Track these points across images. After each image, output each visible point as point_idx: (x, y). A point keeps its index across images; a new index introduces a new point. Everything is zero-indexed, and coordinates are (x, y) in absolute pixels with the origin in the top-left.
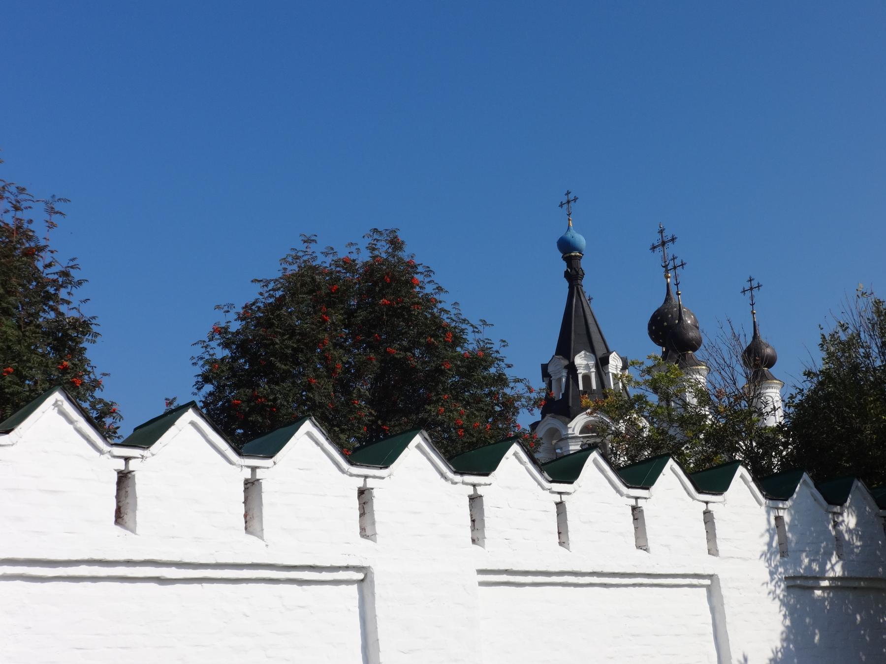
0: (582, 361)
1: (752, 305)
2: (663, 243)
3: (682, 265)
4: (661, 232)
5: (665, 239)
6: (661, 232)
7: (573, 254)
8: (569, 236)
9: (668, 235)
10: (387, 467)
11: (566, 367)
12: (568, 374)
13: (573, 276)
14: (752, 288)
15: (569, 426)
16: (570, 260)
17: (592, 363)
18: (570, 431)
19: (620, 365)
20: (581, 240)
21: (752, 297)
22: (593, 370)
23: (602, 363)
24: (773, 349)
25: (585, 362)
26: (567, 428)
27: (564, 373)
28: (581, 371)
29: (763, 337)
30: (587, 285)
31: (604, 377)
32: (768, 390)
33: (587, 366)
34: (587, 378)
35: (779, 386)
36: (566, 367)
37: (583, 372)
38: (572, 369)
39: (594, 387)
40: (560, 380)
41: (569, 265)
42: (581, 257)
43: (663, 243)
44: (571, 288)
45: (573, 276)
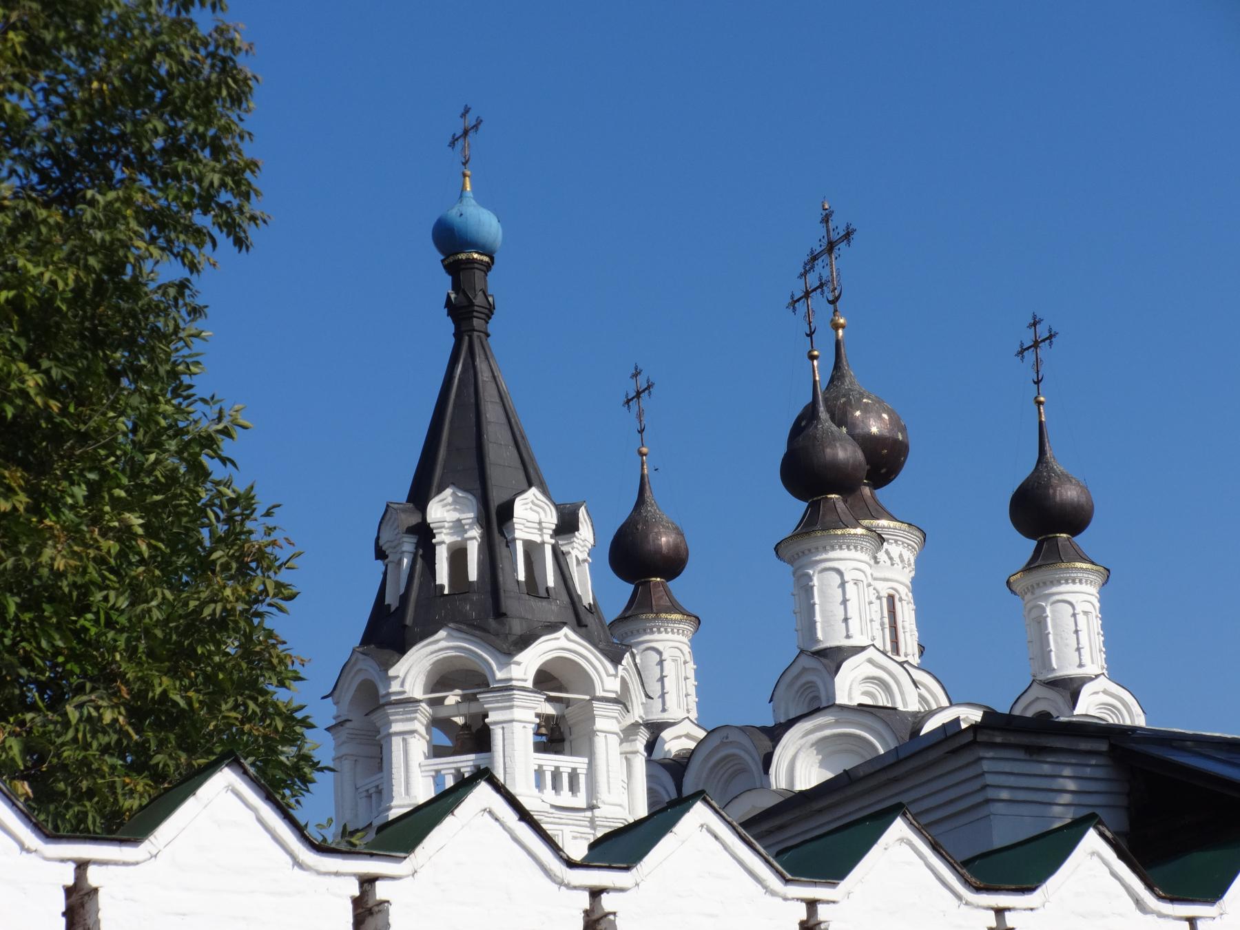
0: (446, 512)
1: (1037, 382)
2: (831, 246)
3: (1050, 337)
4: (826, 220)
5: (834, 236)
6: (826, 220)
7: (463, 256)
8: (453, 213)
9: (838, 223)
10: (627, 869)
11: (411, 530)
12: (417, 546)
13: (466, 313)
14: (1038, 343)
15: (392, 672)
16: (457, 269)
17: (469, 516)
18: (395, 687)
19: (551, 518)
20: (484, 222)
21: (1037, 361)
22: (475, 532)
23: (496, 519)
24: (1084, 489)
25: (455, 516)
26: (389, 680)
27: (409, 544)
28: (444, 540)
29: (1059, 461)
30: (503, 337)
31: (502, 550)
32: (1064, 588)
33: (458, 526)
34: (458, 556)
35: (1100, 581)
36: (411, 530)
37: (448, 539)
38: (424, 535)
39: (473, 575)
40: (400, 562)
41: (456, 286)
42: (488, 267)
43: (831, 246)
44: (458, 335)
45: (466, 313)
